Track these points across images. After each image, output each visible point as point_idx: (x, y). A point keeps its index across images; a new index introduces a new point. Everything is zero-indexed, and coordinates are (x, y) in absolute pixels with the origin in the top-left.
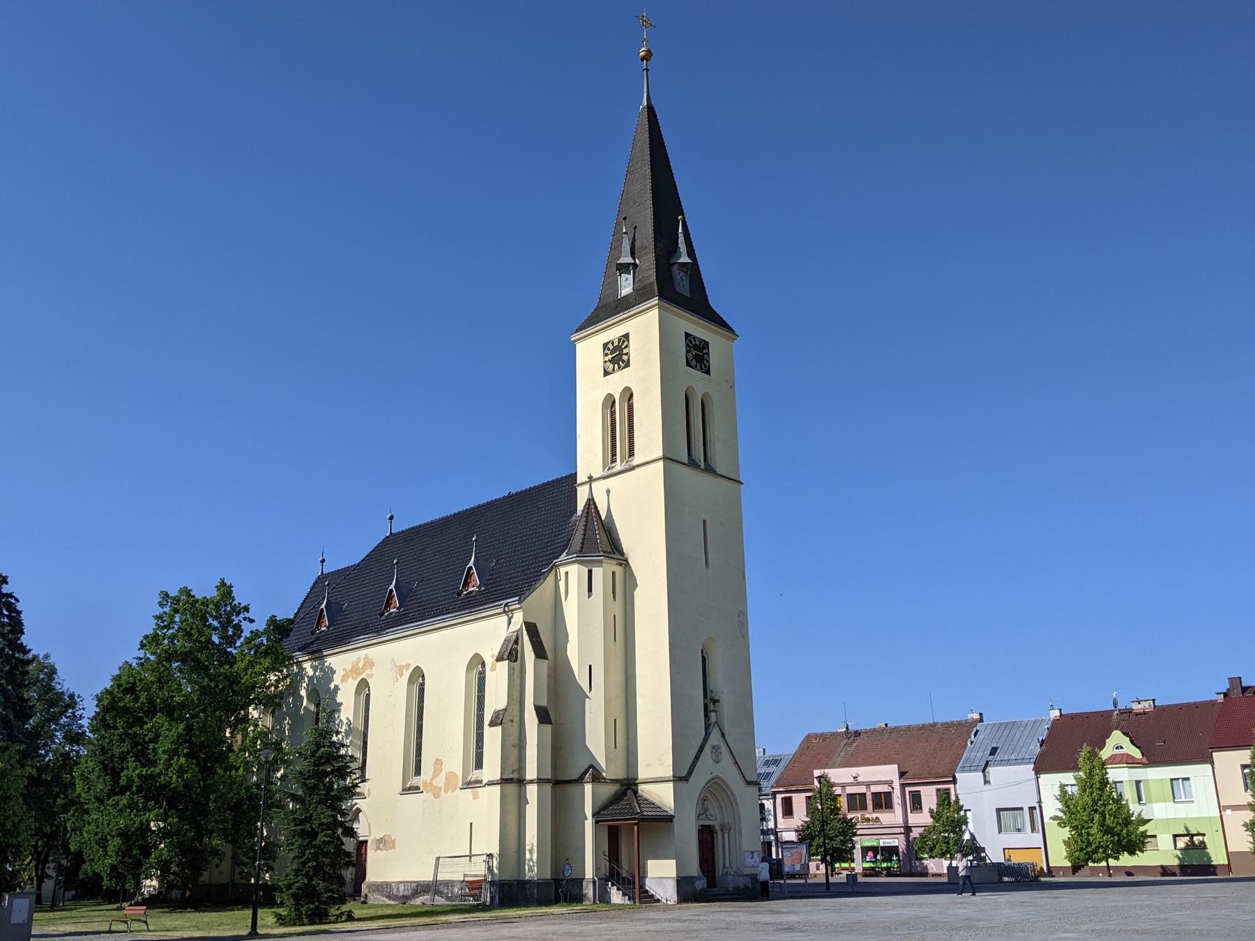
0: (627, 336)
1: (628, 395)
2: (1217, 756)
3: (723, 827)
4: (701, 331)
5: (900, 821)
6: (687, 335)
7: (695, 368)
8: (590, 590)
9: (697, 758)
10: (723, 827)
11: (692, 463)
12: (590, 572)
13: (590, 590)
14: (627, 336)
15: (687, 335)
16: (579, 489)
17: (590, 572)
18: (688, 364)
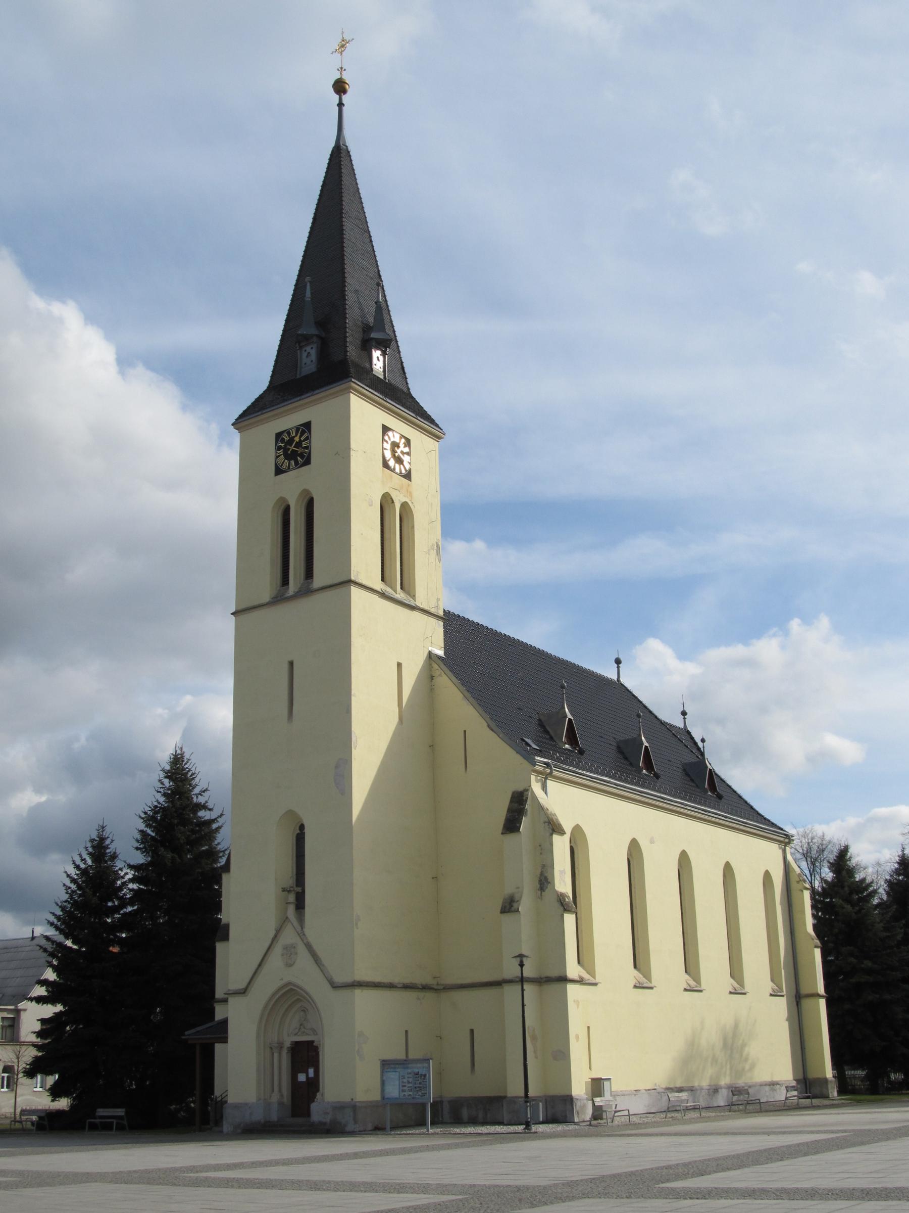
0: (307, 426)
14: (307, 426)
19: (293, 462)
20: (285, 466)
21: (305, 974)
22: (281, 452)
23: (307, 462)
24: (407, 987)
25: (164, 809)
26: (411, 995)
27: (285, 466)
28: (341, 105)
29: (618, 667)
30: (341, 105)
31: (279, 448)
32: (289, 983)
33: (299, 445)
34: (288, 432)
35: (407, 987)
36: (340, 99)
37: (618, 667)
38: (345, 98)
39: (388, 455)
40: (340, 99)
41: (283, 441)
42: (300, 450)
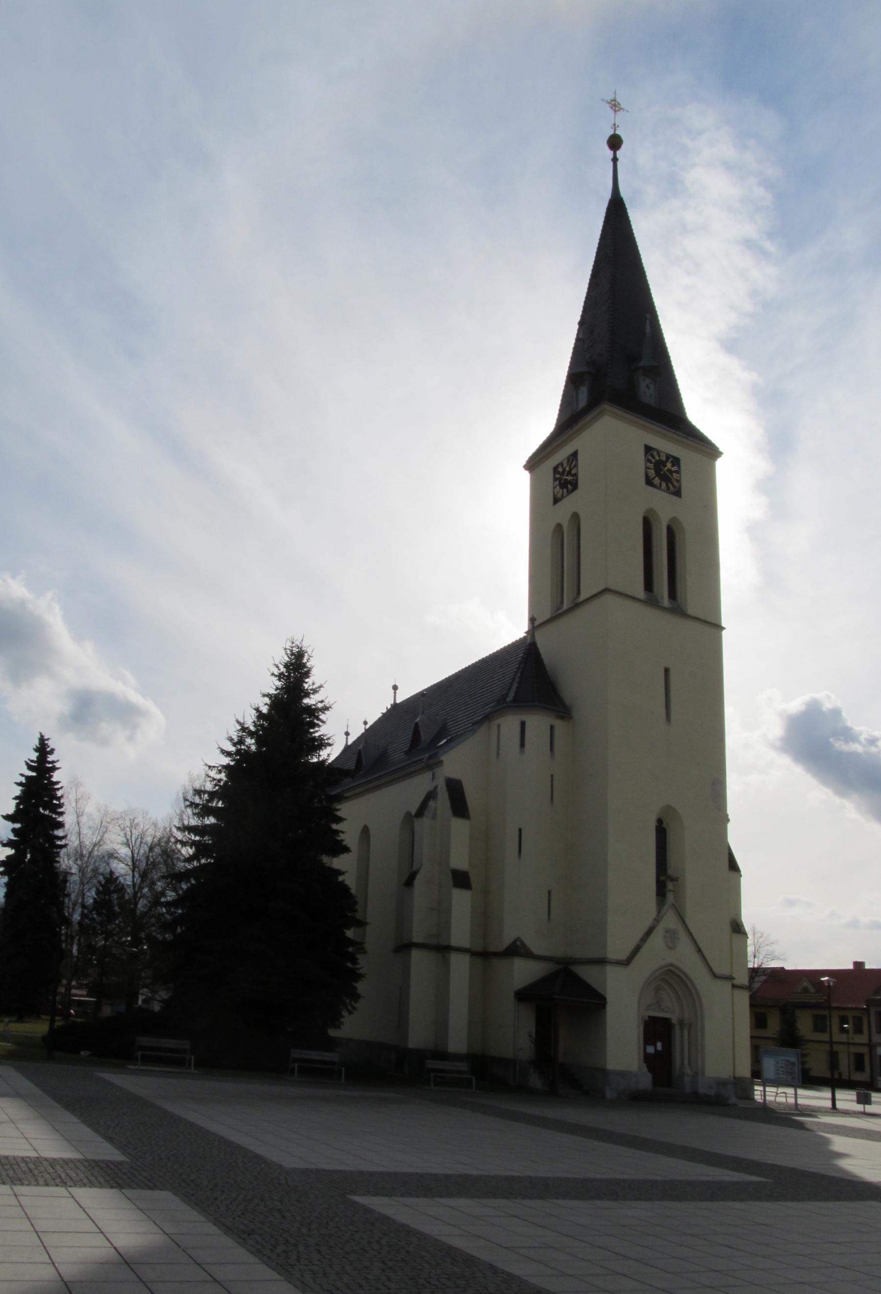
0: (575, 455)
1: (576, 517)
2: (851, 967)
3: (681, 1023)
4: (665, 445)
5: (866, 1041)
6: (648, 449)
7: (659, 488)
8: (522, 744)
9: (699, 951)
10: (681, 1023)
11: (651, 601)
12: (523, 724)
13: (522, 744)
14: (575, 455)
15: (648, 449)
16: (790, 1091)
17: (523, 724)
18: (649, 482)
19: (565, 490)
20: (559, 496)
21: (685, 958)
22: (557, 482)
23: (575, 486)
24: (59, 1274)
25: (110, 882)
26: (66, 1290)
27: (559, 496)
28: (615, 160)
29: (395, 693)
30: (615, 160)
31: (555, 479)
32: (672, 965)
33: (569, 473)
34: (561, 464)
35: (59, 1274)
36: (615, 154)
37: (395, 693)
38: (619, 153)
39: (652, 473)
40: (615, 154)
41: (559, 473)
42: (569, 478)
